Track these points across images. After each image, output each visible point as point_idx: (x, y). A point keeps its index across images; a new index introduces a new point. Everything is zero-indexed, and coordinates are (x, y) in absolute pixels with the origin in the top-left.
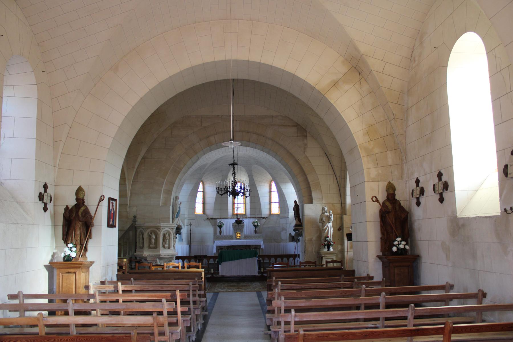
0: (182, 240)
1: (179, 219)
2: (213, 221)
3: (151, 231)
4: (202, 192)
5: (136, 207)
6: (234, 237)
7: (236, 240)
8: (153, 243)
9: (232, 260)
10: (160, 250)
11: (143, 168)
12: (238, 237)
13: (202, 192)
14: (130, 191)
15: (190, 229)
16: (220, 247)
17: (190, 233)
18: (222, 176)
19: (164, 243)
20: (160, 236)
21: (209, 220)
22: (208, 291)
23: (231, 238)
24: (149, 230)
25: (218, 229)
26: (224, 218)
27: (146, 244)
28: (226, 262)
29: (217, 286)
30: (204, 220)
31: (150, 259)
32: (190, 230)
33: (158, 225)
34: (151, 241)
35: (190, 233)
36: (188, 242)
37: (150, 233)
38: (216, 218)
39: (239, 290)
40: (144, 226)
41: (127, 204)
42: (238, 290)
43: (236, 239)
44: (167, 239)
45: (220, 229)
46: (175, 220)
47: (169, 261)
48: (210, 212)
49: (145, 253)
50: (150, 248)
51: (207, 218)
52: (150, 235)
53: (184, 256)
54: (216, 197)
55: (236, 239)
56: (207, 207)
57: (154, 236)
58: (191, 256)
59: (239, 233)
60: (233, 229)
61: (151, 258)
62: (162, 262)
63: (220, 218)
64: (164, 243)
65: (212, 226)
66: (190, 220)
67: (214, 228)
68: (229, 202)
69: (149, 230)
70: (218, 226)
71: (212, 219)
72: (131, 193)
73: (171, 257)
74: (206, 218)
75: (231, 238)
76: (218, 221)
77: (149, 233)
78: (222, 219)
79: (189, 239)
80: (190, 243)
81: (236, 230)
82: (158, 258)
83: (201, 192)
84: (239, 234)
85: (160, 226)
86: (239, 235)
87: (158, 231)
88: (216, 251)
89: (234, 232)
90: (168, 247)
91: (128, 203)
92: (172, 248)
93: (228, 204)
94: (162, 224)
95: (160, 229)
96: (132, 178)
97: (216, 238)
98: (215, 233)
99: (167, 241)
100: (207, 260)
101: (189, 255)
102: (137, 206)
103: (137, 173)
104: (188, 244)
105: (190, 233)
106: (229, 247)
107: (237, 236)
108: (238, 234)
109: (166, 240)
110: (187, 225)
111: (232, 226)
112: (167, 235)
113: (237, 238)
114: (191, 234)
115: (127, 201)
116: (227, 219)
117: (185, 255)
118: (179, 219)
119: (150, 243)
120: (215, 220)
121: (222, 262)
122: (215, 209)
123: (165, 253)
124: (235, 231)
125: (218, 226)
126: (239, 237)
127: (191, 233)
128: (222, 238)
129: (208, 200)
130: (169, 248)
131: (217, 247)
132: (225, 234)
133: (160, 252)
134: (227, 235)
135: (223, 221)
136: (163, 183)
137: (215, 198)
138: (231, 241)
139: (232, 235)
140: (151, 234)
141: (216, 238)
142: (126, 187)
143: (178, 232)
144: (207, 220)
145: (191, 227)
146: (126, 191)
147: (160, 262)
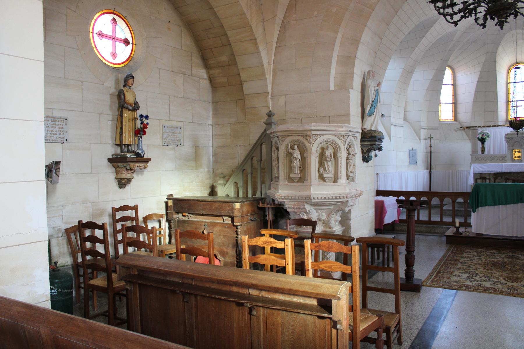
0: (417, 162)
1: (375, 119)
2: (470, 132)
3: (293, 142)
4: (452, 85)
5: (283, 97)
6: (509, 157)
7: (512, 162)
8: (297, 170)
9: (499, 204)
10: (311, 185)
11: (294, 16)
12: (515, 157)
13: (452, 85)
14: (272, 66)
15: (430, 145)
16: (481, 174)
17: (431, 152)
18: (487, 53)
19: (322, 169)
20: (311, 154)
21: (464, 129)
22: (430, 283)
23: (502, 159)
24: (288, 140)
25: (480, 144)
26: (490, 126)
27: (283, 173)
28: (487, 207)
29: (462, 260)
30: (456, 131)
31: (290, 206)
32: (431, 147)
33: (306, 127)
34: (292, 164)
35: (430, 150)
36: (428, 165)
37: (289, 147)
38: (476, 127)
39: (512, 288)
40: (278, 132)
41: (268, 93)
42: (510, 284)
43: (513, 160)
44: (327, 159)
45: (483, 143)
46: (366, 121)
47: (338, 209)
48: (465, 118)
49: (280, 191)
50: (291, 180)
51: (461, 127)
52: (291, 151)
53: (419, 190)
54: (475, 92)
55: (513, 160)
56: (460, 109)
57: (297, 154)
58: (432, 191)
59: (518, 150)
60: (506, 144)
61: (294, 203)
62: (323, 212)
63: (484, 127)
64: (322, 169)
65: (470, 139)
66: (429, 130)
67: (472, 144)
68: (499, 100)
69: (288, 140)
70: (478, 138)
71: (468, 128)
72: (274, 70)
73: (343, 202)
74: (459, 127)
75: (502, 159)
76: (479, 130)
77: (288, 148)
78: (487, 128)
79: (429, 162)
80: (430, 168)
81: (513, 146)
82: (306, 202)
83: (451, 86)
84: (519, 152)
85: (311, 130)
86: (517, 154)
87: (306, 142)
88: (474, 181)
89: (509, 149)
90: (333, 180)
91: (270, 90)
92: (343, 180)
93: (499, 102)
94: (314, 126)
95: (309, 136)
96: (275, 40)
97: (475, 159)
98: (474, 151)
99: (328, 165)
100: (452, 199)
101: (428, 190)
102: (286, 95)
103: (284, 27)
104: (427, 169)
105: (431, 152)
106: (497, 175)
107: (513, 157)
108: (515, 152)
109: (326, 162)
110: (425, 139)
111: (505, 138)
112: (329, 152)
113: (514, 160)
114: (432, 153)
115: (266, 86)
116: (495, 128)
117: (420, 190)
118: (375, 119)
119: (291, 169)
120: (474, 131)
121: (478, 207)
122: (474, 112)
123: (291, 192)
124: (511, 148)
125: (478, 138)
126: (519, 157)
127: (432, 152)
128: (480, 159)
129: (461, 97)
130: (335, 181)
131: (475, 175)
132: (492, 153)
133: (312, 190)
134: (496, 153)
135: (487, 130)
136: (335, 40)
137: (473, 93)
138: (502, 165)
139: (504, 153)
140: (293, 148)
141: (475, 159)
142: (260, 57)
143: (372, 145)
144: (461, 130)
145: (432, 141)
146: (263, 66)
147: (317, 212)
